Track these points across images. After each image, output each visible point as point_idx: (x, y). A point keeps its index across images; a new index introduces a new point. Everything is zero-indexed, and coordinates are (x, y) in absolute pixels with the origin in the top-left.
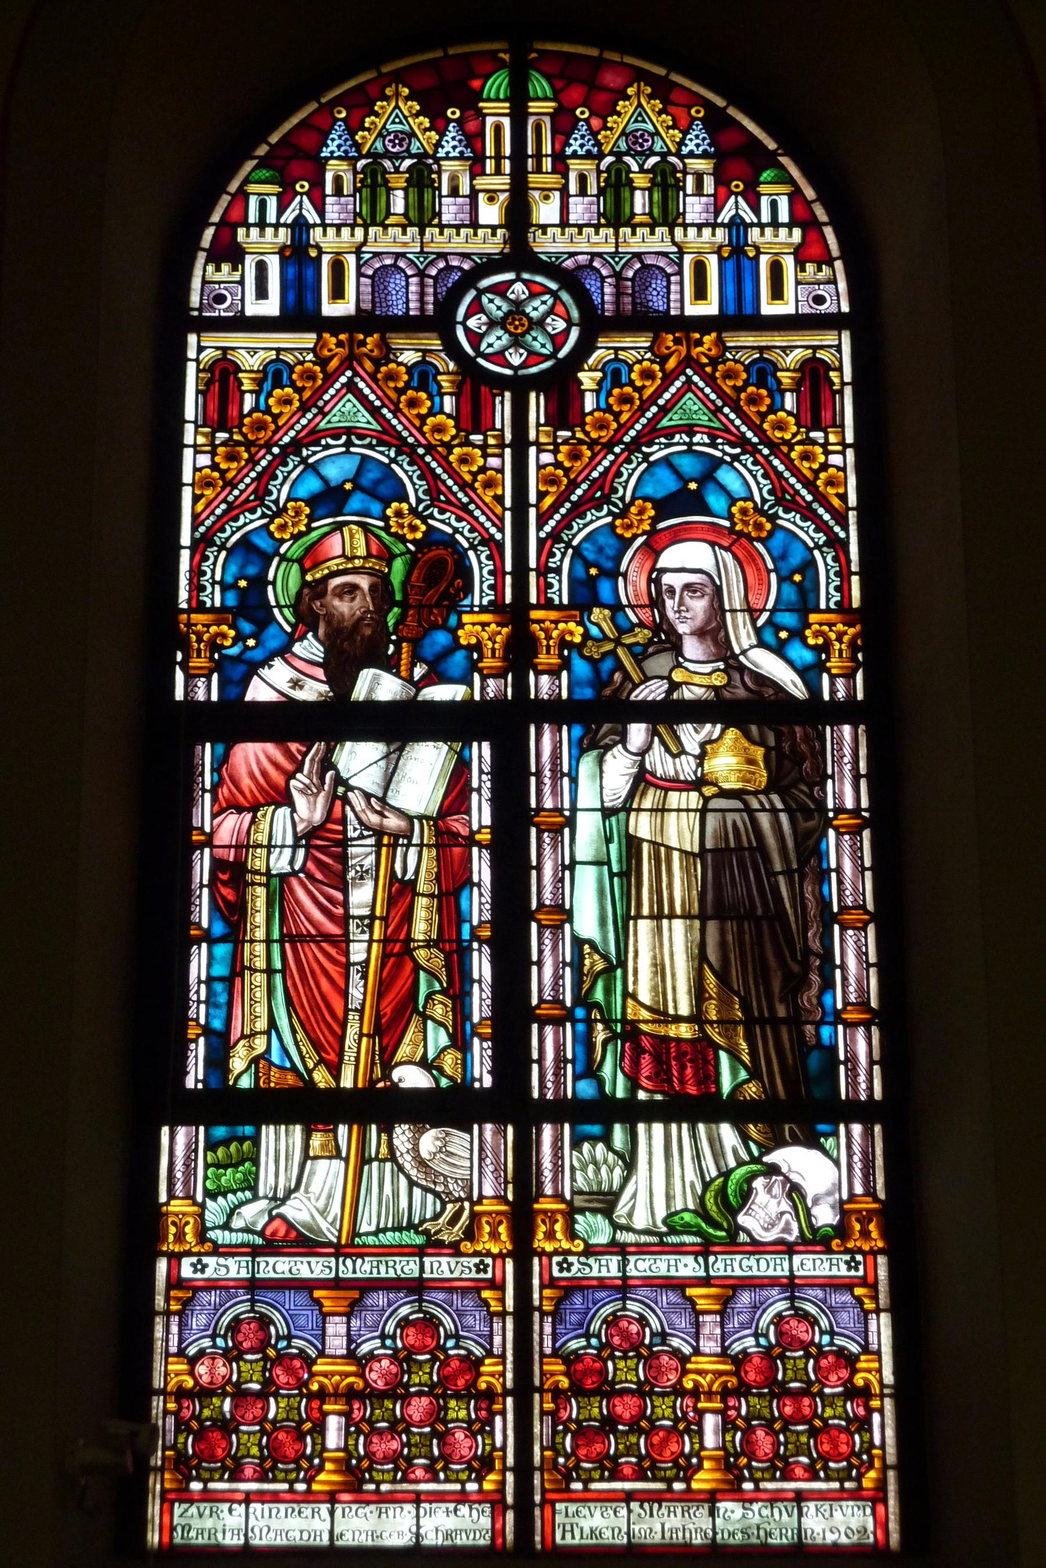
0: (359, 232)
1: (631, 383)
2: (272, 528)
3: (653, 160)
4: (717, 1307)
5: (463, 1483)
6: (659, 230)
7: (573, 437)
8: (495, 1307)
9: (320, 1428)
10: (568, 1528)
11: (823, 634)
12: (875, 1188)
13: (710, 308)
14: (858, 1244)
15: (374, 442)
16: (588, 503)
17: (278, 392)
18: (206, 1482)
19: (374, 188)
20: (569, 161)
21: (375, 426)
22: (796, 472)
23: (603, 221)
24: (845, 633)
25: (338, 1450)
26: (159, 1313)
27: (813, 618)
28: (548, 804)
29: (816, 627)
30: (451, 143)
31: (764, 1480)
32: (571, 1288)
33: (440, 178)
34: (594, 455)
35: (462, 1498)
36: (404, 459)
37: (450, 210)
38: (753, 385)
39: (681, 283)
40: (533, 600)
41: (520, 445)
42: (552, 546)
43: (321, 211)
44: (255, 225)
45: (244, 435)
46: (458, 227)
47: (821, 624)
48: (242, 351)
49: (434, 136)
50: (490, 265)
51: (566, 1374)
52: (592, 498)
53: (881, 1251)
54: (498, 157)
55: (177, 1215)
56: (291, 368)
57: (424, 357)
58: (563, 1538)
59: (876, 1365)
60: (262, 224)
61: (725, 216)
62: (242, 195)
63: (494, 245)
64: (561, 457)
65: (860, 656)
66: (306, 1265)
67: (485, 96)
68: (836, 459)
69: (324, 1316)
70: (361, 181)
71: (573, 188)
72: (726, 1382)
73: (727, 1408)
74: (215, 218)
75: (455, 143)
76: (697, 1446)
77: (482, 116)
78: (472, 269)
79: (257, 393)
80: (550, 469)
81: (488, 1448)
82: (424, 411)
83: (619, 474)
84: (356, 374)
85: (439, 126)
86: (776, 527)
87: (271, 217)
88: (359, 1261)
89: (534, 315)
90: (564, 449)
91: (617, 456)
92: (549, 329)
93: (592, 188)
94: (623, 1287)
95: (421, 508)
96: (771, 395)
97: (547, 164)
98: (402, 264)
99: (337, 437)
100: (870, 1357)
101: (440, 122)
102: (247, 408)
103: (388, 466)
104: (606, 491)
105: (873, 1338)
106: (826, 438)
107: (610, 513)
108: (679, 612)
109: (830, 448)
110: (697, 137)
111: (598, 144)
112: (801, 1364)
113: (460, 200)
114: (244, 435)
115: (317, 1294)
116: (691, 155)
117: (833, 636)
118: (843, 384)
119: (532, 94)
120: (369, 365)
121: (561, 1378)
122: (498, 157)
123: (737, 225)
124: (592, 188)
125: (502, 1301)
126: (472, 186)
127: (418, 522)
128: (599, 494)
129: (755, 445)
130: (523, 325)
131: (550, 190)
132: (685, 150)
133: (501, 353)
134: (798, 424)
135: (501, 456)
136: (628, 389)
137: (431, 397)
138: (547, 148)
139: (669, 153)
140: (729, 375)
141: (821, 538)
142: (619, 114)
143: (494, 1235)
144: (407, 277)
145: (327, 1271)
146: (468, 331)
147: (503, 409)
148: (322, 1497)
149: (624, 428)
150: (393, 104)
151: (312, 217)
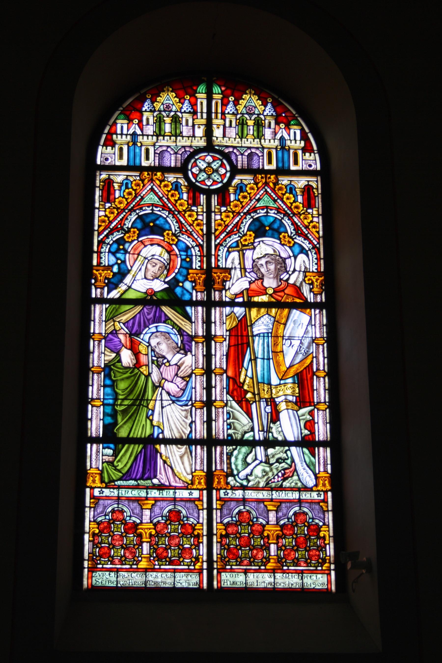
0: (155, 138)
1: (132, 188)
2: (242, 240)
3: (172, 114)
4: (275, 509)
5: (260, 566)
6: (256, 140)
7: (227, 210)
8: (200, 507)
9: (268, 549)
10: (226, 581)
11: (311, 280)
12: (327, 469)
13: (273, 167)
14: (322, 488)
15: (161, 209)
16: (116, 229)
17: (242, 194)
18: (288, 567)
19: (160, 122)
20: (144, 113)
21: (161, 204)
22: (187, 221)
23: (155, 134)
24: (319, 279)
25: (274, 556)
26: (330, 511)
27: (190, 271)
28: (97, 331)
29: (309, 277)
30: (186, 107)
31: (290, 566)
32: (224, 501)
33: (182, 120)
34: (234, 216)
35: (190, 571)
36: (171, 216)
37: (186, 131)
38: (173, 190)
39: (263, 159)
40: (213, 266)
41: (209, 212)
42: (219, 247)
43: (142, 130)
44: (119, 134)
45: (231, 209)
46: (188, 137)
47: (310, 276)
48: (296, 182)
49: (263, 107)
50: (199, 150)
51: (98, 528)
52: (117, 228)
53: (205, 489)
54: (202, 113)
55: (198, 476)
56: (246, 186)
57: (291, 182)
58: (224, 584)
59: (328, 529)
60: (122, 134)
61: (278, 136)
62: (115, 124)
63: (202, 143)
64: (107, 213)
65: (323, 288)
66: (309, 494)
67: (198, 92)
68: (315, 219)
69: (268, 511)
70: (156, 120)
71: (227, 124)
72: (151, 532)
73: (151, 541)
74: (106, 131)
75: (149, 106)
76: (140, 554)
77: (197, 99)
78: (193, 152)
79: (120, 190)
80: (103, 217)
81: (197, 554)
82: (292, 201)
83: (242, 223)
84: (154, 185)
85: (182, 100)
86: (179, 240)
87: (125, 132)
88: (281, 492)
89: (215, 167)
90: (108, 210)
91: (126, 213)
92: (220, 173)
93: (234, 124)
94: (244, 501)
95: (292, 235)
96: (294, 196)
97: (219, 116)
98: (169, 150)
99: (263, 209)
100: (326, 526)
101: (182, 101)
102: (117, 196)
103: (139, 216)
104: (122, 225)
105: (326, 520)
106: (312, 212)
107: (239, 236)
108: (268, 271)
109: (199, 213)
110: (149, 104)
111: (154, 107)
112: (119, 526)
113: (189, 128)
114: (231, 209)
115: (266, 503)
116: (185, 112)
117: (197, 278)
118: (318, 194)
119: (214, 92)
120: (158, 182)
121: (223, 530)
122: (202, 113)
123: (134, 135)
124: (234, 124)
125: (327, 507)
126: (193, 123)
127: (291, 240)
128: (299, 232)
129: (173, 211)
130: (210, 171)
131: (220, 125)
132: (183, 111)
133: (204, 181)
134: (303, 207)
135: (202, 215)
136: (246, 194)
137: (179, 194)
138: (219, 110)
139: (178, 111)
140: (280, 189)
141: (194, 244)
142: (244, 99)
143: (324, 485)
144: (171, 154)
145: (269, 495)
146: (192, 173)
147: (203, 198)
148: (270, 571)
149: (128, 204)
150: (249, 96)
151: (139, 132)
